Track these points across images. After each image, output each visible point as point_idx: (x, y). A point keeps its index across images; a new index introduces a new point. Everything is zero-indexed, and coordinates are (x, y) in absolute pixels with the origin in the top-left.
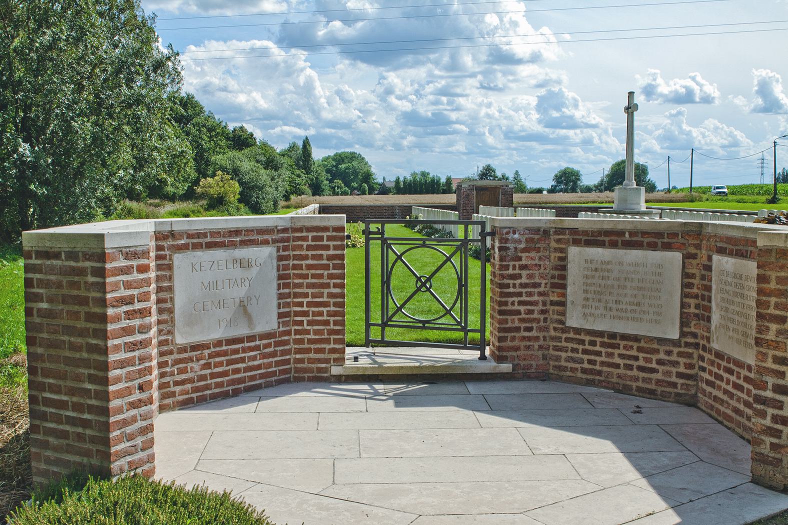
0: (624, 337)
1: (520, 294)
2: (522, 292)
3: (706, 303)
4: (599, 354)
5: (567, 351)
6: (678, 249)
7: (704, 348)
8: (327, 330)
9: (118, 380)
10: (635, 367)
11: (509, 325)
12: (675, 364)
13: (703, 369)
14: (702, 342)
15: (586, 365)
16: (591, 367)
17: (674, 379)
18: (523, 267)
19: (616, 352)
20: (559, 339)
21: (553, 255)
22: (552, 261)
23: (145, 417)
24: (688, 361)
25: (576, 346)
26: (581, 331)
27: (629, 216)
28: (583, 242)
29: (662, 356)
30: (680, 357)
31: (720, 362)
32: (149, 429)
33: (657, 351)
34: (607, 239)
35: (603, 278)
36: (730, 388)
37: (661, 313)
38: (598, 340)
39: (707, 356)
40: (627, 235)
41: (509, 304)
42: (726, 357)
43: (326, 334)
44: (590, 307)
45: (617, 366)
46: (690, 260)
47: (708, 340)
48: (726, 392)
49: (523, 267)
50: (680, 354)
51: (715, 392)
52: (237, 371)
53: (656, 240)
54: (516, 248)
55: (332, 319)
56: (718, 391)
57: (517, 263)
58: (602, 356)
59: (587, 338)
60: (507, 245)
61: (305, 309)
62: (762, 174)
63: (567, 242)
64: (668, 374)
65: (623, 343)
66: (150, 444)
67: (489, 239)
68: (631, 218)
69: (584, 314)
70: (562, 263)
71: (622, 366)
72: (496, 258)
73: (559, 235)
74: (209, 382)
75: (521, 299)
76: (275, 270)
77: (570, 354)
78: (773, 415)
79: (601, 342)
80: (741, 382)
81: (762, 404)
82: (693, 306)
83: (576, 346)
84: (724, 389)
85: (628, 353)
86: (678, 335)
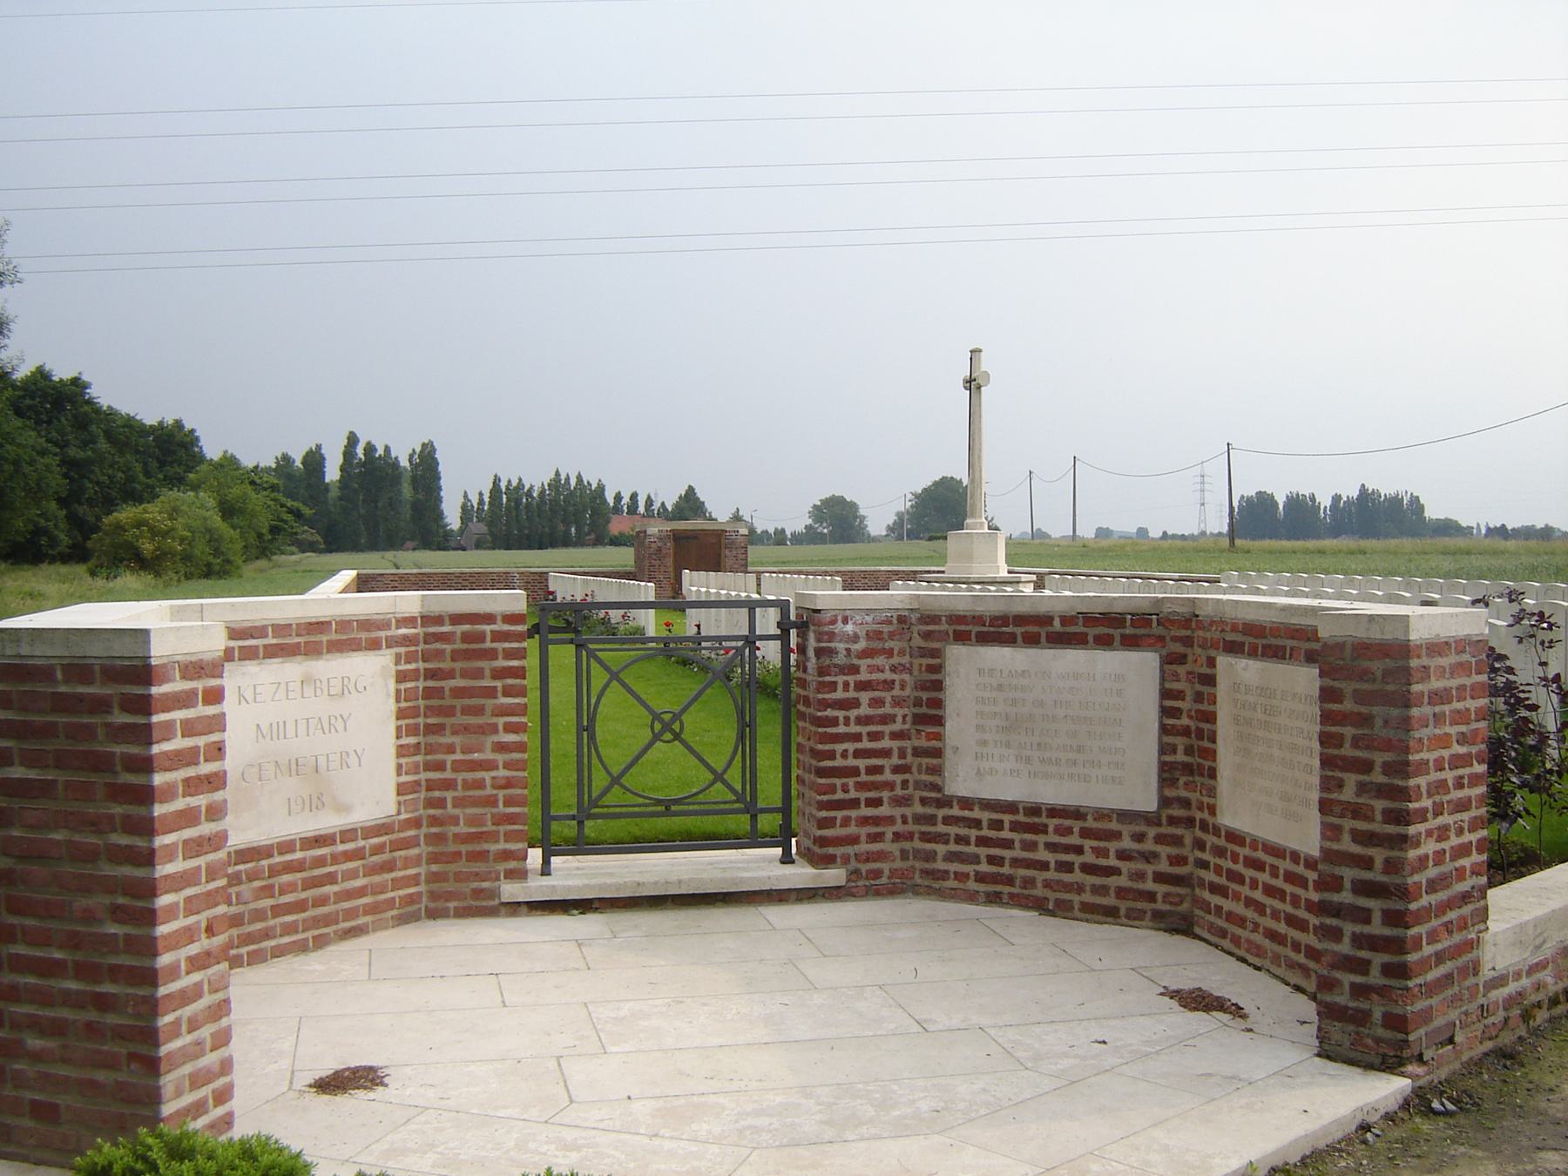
0: (1054, 812)
1: (857, 737)
2: (860, 734)
3: (1206, 744)
4: (1008, 844)
5: (947, 842)
6: (1150, 647)
7: (1204, 826)
8: (493, 815)
9: (172, 912)
10: (1076, 866)
11: (840, 795)
12: (1150, 857)
13: (1204, 865)
14: (1199, 815)
15: (984, 867)
16: (993, 869)
17: (1150, 885)
18: (863, 686)
19: (1041, 839)
20: (931, 820)
21: (917, 662)
22: (916, 673)
23: (220, 985)
24: (1174, 851)
25: (963, 831)
26: (973, 804)
27: (992, 588)
28: (973, 636)
29: (1127, 843)
30: (1161, 844)
31: (1237, 849)
32: (222, 1008)
33: (1117, 835)
34: (1019, 630)
35: (1014, 702)
36: (1258, 895)
37: (1123, 765)
38: (1007, 818)
39: (1210, 839)
40: (1057, 623)
41: (838, 756)
42: (1248, 840)
43: (489, 823)
44: (990, 756)
45: (1044, 866)
46: (1174, 667)
47: (1212, 810)
48: (1249, 902)
49: (863, 686)
50: (1160, 839)
51: (1228, 905)
52: (321, 901)
53: (1111, 631)
54: (848, 650)
55: (501, 794)
56: (1234, 903)
57: (851, 679)
58: (1014, 849)
59: (985, 816)
60: (832, 645)
61: (448, 774)
62: (1203, 504)
63: (943, 637)
64: (1141, 876)
65: (1052, 823)
66: (222, 1039)
67: (793, 632)
68: (995, 591)
69: (979, 769)
70: (934, 677)
71: (1052, 865)
72: (810, 670)
73: (928, 624)
74: (271, 923)
75: (859, 745)
76: (392, 700)
77: (953, 847)
78: (1354, 934)
79: (1011, 822)
80: (1279, 883)
81: (1333, 916)
82: (1181, 749)
83: (963, 831)
84: (1246, 897)
85: (1063, 840)
86: (1156, 805)
